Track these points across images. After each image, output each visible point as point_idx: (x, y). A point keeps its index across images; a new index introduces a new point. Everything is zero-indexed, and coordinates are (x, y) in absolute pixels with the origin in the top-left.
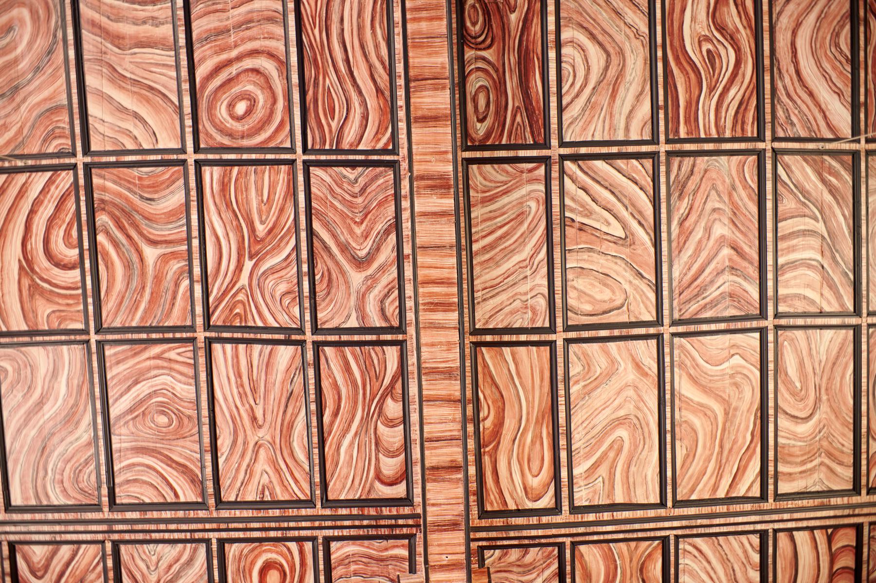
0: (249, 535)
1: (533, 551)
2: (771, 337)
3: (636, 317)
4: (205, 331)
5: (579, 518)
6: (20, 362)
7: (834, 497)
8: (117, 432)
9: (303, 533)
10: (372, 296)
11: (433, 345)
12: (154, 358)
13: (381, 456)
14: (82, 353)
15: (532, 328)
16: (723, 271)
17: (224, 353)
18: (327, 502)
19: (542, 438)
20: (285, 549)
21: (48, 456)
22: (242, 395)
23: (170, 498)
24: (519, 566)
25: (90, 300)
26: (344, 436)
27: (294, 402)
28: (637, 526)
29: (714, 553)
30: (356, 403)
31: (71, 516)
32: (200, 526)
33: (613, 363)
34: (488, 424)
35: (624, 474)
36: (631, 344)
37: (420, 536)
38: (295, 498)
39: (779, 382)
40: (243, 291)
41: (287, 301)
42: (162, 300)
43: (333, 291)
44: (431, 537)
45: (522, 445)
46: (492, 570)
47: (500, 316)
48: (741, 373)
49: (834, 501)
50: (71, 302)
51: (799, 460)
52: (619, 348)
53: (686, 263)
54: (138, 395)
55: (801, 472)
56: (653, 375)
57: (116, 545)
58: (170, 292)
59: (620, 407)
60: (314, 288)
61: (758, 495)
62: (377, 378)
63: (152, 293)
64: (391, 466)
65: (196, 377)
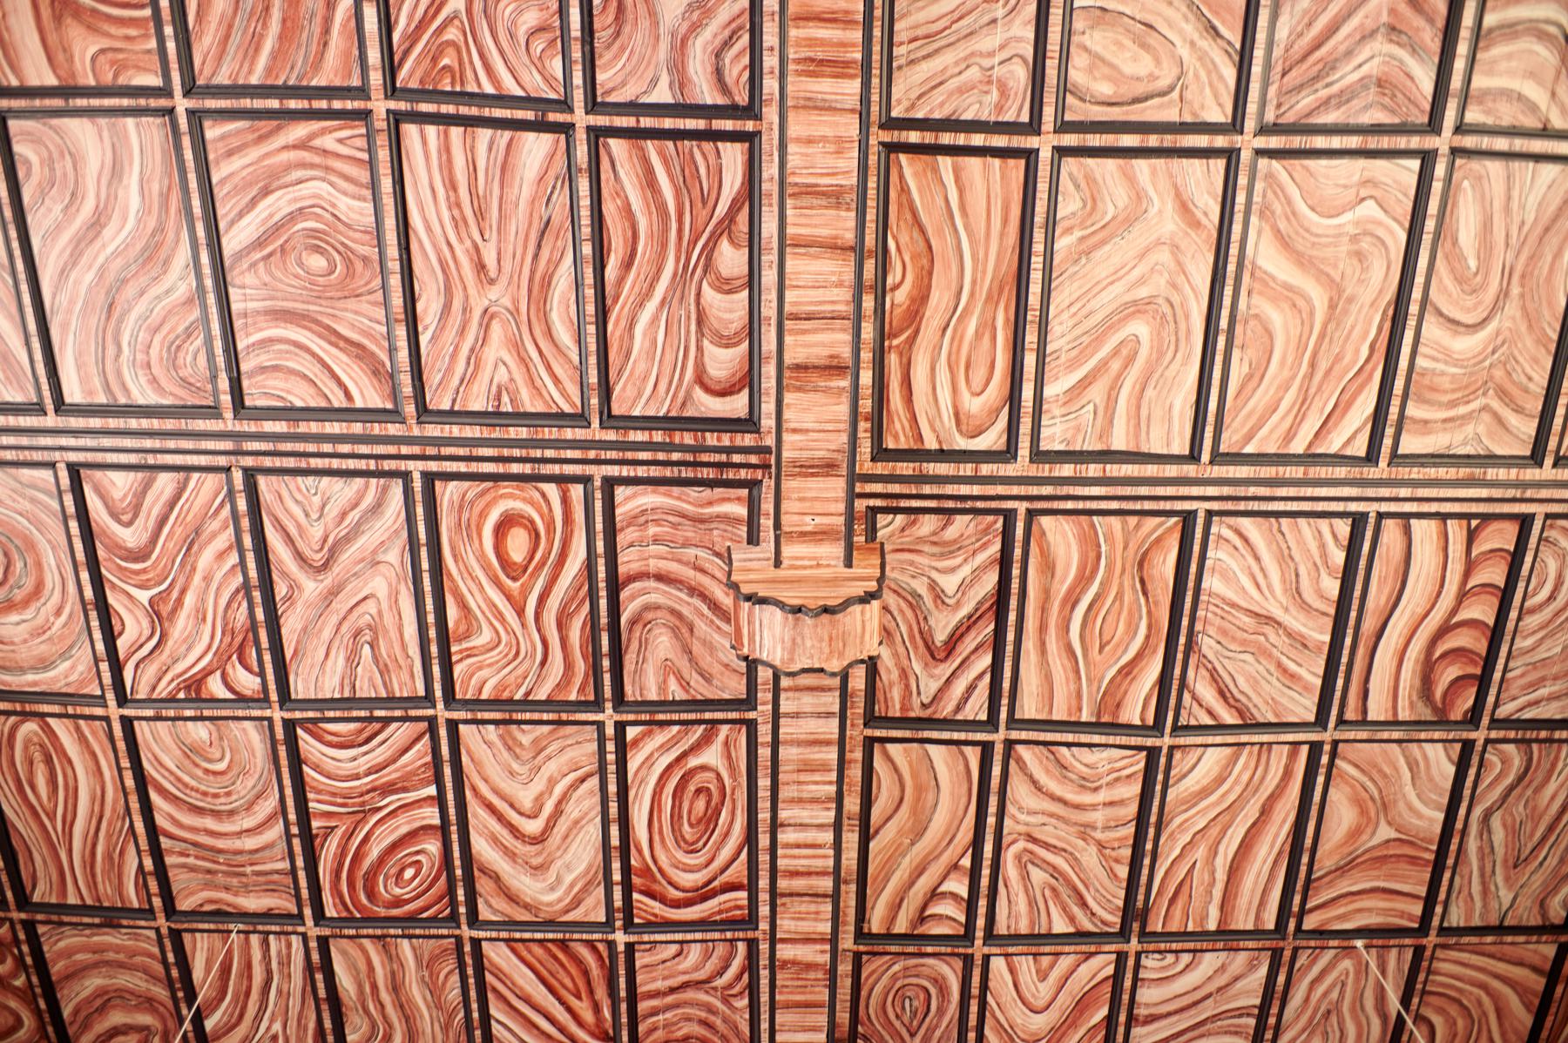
0: (474, 467)
1: (961, 521)
2: (1440, 170)
3: (1194, 114)
4: (386, 98)
5: (1045, 470)
6: (52, 148)
7: (1494, 466)
8: (237, 281)
9: (569, 469)
10: (699, 42)
11: (810, 141)
12: (295, 147)
13: (706, 343)
14: (162, 133)
15: (997, 123)
16: (1373, 33)
17: (424, 142)
18: (609, 419)
19: (994, 328)
20: (537, 495)
21: (120, 321)
22: (459, 223)
23: (338, 401)
24: (935, 543)
25: (168, 30)
26: (641, 305)
27: (552, 240)
28: (1143, 491)
29: (1269, 545)
30: (664, 245)
31: (170, 424)
32: (392, 450)
33: (1139, 198)
34: (900, 298)
35: (1134, 401)
36: (1178, 164)
37: (768, 485)
38: (554, 410)
39: (1439, 255)
40: (456, 22)
41: (538, 46)
42: (305, 35)
43: (627, 29)
44: (787, 484)
45: (957, 339)
46: (887, 548)
47: (938, 96)
48: (1372, 235)
49: (1492, 473)
50: (133, 32)
51: (1445, 398)
52: (1154, 172)
53: (1306, 12)
54: (271, 216)
55: (1445, 421)
56: (1210, 226)
57: (250, 475)
58: (318, 20)
59: (1141, 281)
60: (591, 23)
61: (1362, 453)
62: (704, 203)
63: (284, 21)
64: (723, 361)
65: (374, 185)
